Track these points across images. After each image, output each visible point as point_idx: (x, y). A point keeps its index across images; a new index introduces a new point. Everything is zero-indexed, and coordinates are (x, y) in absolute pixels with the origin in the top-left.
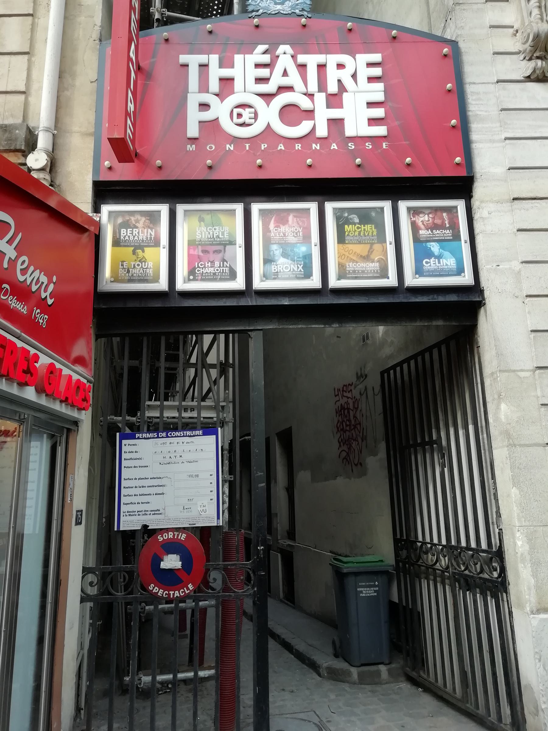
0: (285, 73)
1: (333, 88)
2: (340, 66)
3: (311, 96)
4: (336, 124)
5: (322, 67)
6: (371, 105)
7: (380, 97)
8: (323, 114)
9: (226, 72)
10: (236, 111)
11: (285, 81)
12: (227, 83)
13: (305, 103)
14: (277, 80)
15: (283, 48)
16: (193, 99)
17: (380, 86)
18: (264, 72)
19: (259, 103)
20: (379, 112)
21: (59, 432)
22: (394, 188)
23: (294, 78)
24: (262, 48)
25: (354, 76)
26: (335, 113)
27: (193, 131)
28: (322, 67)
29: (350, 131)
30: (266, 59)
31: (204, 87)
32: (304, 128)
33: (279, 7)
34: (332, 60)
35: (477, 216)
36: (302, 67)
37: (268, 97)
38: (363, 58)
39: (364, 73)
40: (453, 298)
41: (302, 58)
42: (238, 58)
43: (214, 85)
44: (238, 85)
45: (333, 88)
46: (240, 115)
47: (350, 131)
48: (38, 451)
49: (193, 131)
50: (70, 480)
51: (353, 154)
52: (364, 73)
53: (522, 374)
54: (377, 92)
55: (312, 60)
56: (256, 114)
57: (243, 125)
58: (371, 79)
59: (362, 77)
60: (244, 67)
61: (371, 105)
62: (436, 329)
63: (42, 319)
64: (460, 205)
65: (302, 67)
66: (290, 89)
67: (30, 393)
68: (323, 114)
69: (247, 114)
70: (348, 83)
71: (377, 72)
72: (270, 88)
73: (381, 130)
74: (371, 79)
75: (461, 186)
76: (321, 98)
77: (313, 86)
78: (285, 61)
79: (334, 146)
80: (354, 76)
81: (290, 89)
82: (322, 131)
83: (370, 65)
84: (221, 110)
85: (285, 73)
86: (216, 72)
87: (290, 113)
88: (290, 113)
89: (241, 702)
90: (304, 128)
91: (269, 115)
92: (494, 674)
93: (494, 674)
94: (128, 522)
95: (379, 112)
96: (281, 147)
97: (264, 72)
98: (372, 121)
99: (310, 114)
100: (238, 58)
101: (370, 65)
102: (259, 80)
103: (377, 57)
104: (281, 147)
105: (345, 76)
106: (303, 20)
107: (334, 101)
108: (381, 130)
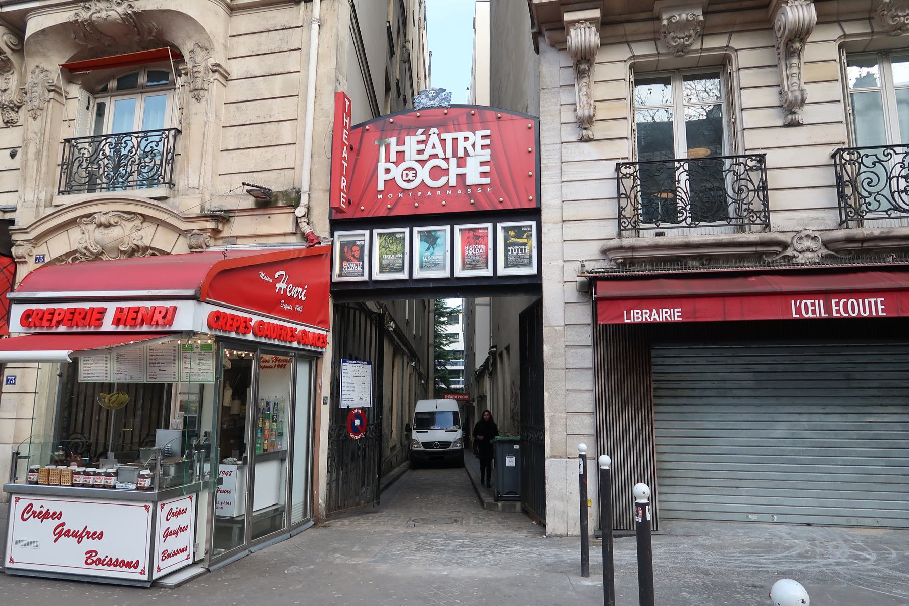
0: (434, 147)
1: (461, 153)
2: (466, 139)
3: (447, 159)
4: (461, 177)
5: (455, 140)
6: (482, 163)
7: (488, 158)
8: (454, 171)
9: (400, 148)
10: (405, 172)
11: (434, 152)
12: (400, 154)
13: (444, 165)
14: (429, 151)
15: (433, 130)
16: (382, 165)
17: (488, 151)
18: (422, 147)
19: (417, 166)
20: (487, 169)
21: (313, 358)
22: (495, 216)
23: (439, 150)
24: (420, 131)
25: (473, 145)
26: (461, 171)
27: (381, 186)
28: (455, 140)
29: (469, 182)
30: (423, 138)
31: (388, 159)
32: (443, 181)
33: (432, 102)
34: (461, 136)
35: (544, 230)
36: (443, 142)
37: (422, 162)
38: (479, 133)
39: (480, 142)
40: (526, 282)
41: (443, 136)
42: (407, 139)
43: (393, 157)
44: (406, 157)
45: (461, 153)
46: (407, 175)
47: (469, 182)
48: (303, 370)
49: (381, 186)
50: (319, 381)
51: (470, 196)
52: (480, 142)
53: (557, 328)
54: (486, 155)
55: (449, 137)
56: (416, 173)
57: (409, 181)
58: (483, 147)
59: (478, 147)
60: (411, 144)
61: (482, 163)
62: (517, 303)
63: (299, 308)
64: (534, 224)
65: (443, 142)
66: (435, 156)
67: (295, 345)
68: (454, 171)
69: (411, 174)
70: (470, 150)
71: (487, 142)
72: (425, 156)
73: (487, 180)
74: (483, 147)
75: (535, 213)
76: (453, 161)
77: (449, 153)
78: (434, 139)
79: (459, 192)
80: (473, 145)
81: (435, 156)
82: (453, 183)
83: (484, 137)
84: (397, 173)
85: (434, 147)
86: (394, 148)
87: (436, 172)
88: (436, 172)
89: (211, 37)
90: (443, 181)
91: (423, 174)
92: (371, 337)
93: (371, 337)
94: (344, 405)
95: (487, 169)
96: (429, 193)
97: (422, 147)
98: (483, 174)
99: (446, 171)
100: (407, 139)
101: (484, 137)
102: (420, 152)
103: (488, 132)
104: (429, 193)
105: (468, 145)
106: (446, 111)
107: (461, 162)
108: (487, 180)
